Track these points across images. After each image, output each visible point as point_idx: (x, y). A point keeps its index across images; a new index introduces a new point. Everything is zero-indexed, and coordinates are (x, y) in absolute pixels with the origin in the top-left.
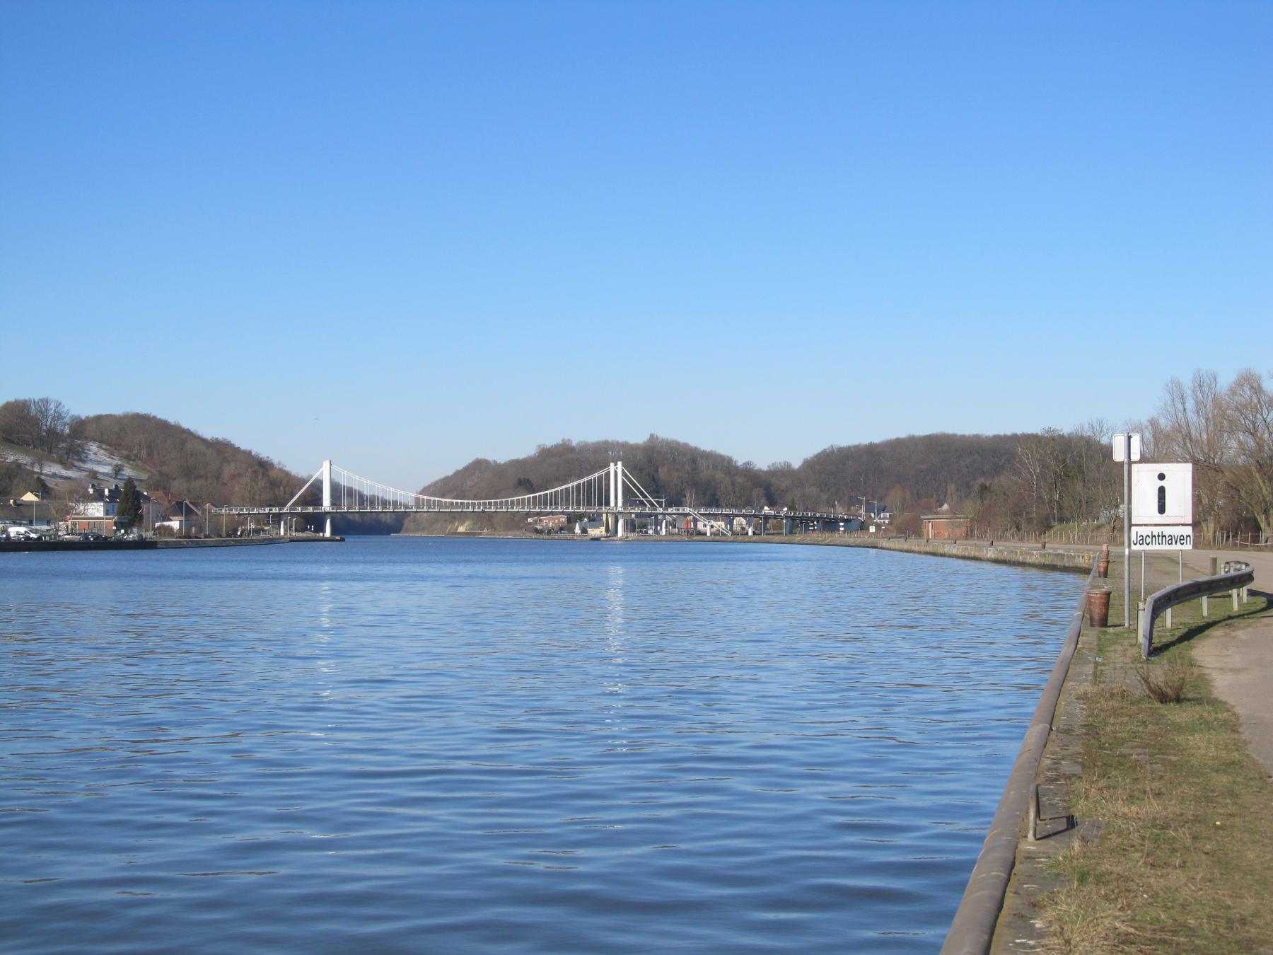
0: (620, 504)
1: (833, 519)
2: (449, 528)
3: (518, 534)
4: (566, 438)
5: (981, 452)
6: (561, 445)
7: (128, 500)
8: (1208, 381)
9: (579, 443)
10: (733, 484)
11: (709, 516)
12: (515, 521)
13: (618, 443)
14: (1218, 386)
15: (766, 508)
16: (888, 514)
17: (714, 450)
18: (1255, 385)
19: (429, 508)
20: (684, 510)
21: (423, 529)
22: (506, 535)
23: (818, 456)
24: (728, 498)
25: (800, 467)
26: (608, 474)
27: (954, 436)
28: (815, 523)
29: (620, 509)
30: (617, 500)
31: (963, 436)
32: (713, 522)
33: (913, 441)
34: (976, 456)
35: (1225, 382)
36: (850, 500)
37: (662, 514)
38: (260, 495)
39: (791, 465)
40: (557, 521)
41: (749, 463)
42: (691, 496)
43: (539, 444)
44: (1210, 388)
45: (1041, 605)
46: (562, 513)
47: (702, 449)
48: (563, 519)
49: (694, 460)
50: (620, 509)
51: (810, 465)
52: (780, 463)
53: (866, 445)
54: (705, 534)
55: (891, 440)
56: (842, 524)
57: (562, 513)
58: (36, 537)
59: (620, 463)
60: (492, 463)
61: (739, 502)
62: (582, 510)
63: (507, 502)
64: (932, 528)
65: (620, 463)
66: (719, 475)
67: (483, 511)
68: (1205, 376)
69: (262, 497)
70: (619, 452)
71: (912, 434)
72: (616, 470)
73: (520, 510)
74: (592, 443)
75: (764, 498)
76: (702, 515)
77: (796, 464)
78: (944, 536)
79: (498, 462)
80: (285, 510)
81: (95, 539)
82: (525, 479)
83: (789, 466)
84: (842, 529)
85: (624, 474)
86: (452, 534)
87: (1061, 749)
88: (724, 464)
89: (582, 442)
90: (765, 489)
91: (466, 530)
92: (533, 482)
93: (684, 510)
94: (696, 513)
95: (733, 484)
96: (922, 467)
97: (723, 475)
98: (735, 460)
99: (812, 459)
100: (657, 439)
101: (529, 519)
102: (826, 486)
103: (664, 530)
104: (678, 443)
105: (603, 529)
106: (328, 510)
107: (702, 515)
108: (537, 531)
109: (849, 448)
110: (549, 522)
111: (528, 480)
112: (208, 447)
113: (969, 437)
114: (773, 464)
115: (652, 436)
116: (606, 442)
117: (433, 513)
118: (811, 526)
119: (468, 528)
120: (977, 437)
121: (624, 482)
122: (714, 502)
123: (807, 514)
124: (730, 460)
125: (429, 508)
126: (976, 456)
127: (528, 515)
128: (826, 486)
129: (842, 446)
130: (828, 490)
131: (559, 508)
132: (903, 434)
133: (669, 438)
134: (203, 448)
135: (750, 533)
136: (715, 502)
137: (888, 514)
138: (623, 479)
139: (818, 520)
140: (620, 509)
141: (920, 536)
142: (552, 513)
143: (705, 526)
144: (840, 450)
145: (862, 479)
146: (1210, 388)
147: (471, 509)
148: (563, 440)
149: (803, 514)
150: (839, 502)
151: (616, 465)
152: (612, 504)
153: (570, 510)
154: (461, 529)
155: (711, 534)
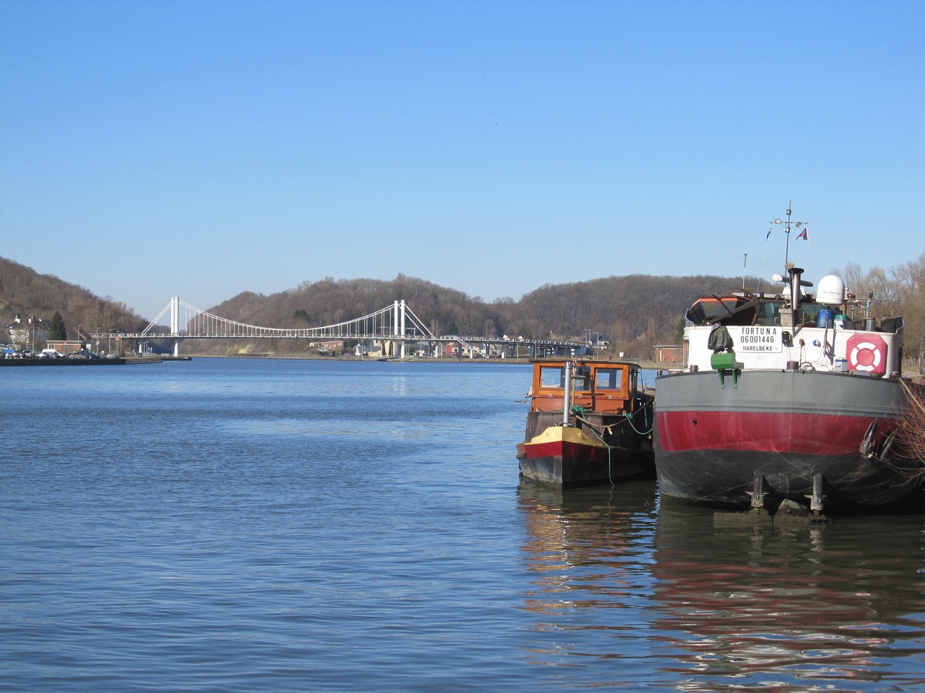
0: (403, 332)
1: (566, 346)
2: (229, 350)
3: (307, 356)
4: (329, 276)
5: (671, 291)
6: (324, 282)
7: (56, 328)
8: (855, 270)
9: (340, 281)
10: (468, 316)
11: (471, 343)
12: (298, 345)
13: (372, 281)
14: (861, 272)
15: (505, 337)
16: (603, 342)
17: (451, 287)
18: (881, 275)
19: (211, 334)
20: (443, 338)
21: (201, 351)
22: (294, 356)
23: (535, 293)
24: (464, 327)
25: (520, 302)
26: (393, 310)
27: (648, 277)
28: (553, 349)
29: (403, 337)
30: (399, 330)
31: (657, 278)
32: (475, 348)
33: (614, 280)
34: (668, 294)
35: (865, 272)
36: (563, 330)
37: (436, 341)
38: (106, 323)
39: (512, 300)
40: (335, 346)
41: (478, 298)
42: (435, 326)
43: (305, 280)
44: (856, 274)
45: (557, 582)
46: (341, 339)
47: (441, 286)
48: (341, 344)
49: (435, 296)
50: (403, 337)
51: (529, 300)
52: (504, 298)
53: (574, 284)
54: (469, 357)
55: (596, 280)
56: (573, 350)
57: (341, 339)
58: (62, 356)
59: (403, 302)
60: (258, 295)
61: (473, 331)
62: (356, 337)
63: (297, 331)
64: (662, 354)
65: (403, 302)
66: (457, 308)
67: (297, 338)
68: (853, 267)
69: (108, 324)
70: (373, 288)
71: (613, 275)
72: (400, 307)
73: (282, 337)
74: (351, 281)
75: (494, 327)
76: (466, 342)
77: (517, 299)
78: (671, 359)
79: (264, 294)
80: (143, 335)
81: (93, 357)
82: (301, 310)
83: (511, 300)
84: (573, 354)
85: (406, 311)
86: (236, 355)
87: (727, 686)
88: (459, 299)
89: (342, 279)
90: (494, 320)
91: (248, 352)
92: (308, 312)
93: (452, 338)
94: (462, 340)
95: (468, 316)
96: (622, 303)
97: (460, 309)
98: (468, 296)
99: (530, 295)
100: (404, 277)
101: (310, 344)
102: (542, 318)
103: (436, 353)
104: (421, 281)
105: (380, 352)
106: (176, 336)
107: (466, 342)
108: (322, 354)
109: (560, 286)
110: (329, 346)
111: (304, 311)
112: (51, 283)
113: (661, 278)
114: (498, 299)
115: (400, 275)
116: (363, 280)
117: (205, 339)
118: (549, 351)
119: (249, 350)
120: (668, 278)
121: (406, 318)
122: (453, 331)
123: (547, 342)
124: (464, 296)
125: (211, 334)
126: (668, 294)
127: (309, 340)
128: (542, 318)
129: (555, 284)
130: (545, 322)
131: (347, 335)
132: (606, 275)
133: (414, 277)
134: (47, 284)
135: (503, 357)
136: (454, 331)
137: (603, 342)
138: (405, 315)
139: (555, 346)
140: (403, 337)
141: (651, 359)
142: (332, 339)
143: (469, 351)
144: (554, 288)
145: (572, 312)
146: (856, 274)
147: (287, 336)
148: (326, 278)
149: (544, 342)
150: (553, 331)
151: (399, 302)
152: (396, 333)
153: (347, 337)
154: (243, 351)
155: (473, 357)
